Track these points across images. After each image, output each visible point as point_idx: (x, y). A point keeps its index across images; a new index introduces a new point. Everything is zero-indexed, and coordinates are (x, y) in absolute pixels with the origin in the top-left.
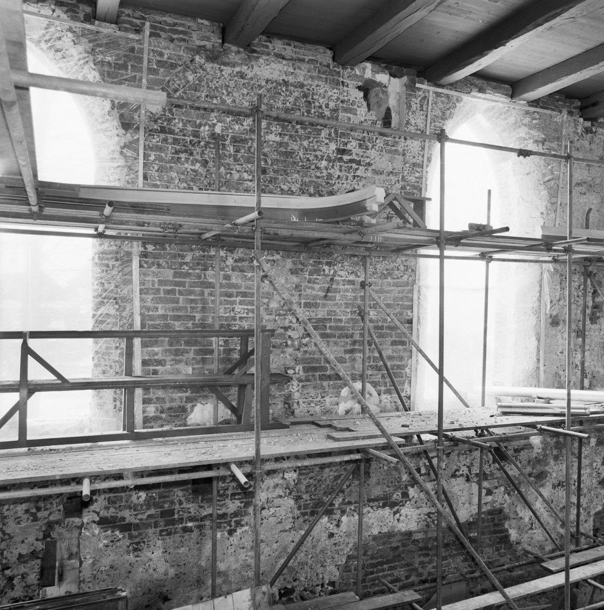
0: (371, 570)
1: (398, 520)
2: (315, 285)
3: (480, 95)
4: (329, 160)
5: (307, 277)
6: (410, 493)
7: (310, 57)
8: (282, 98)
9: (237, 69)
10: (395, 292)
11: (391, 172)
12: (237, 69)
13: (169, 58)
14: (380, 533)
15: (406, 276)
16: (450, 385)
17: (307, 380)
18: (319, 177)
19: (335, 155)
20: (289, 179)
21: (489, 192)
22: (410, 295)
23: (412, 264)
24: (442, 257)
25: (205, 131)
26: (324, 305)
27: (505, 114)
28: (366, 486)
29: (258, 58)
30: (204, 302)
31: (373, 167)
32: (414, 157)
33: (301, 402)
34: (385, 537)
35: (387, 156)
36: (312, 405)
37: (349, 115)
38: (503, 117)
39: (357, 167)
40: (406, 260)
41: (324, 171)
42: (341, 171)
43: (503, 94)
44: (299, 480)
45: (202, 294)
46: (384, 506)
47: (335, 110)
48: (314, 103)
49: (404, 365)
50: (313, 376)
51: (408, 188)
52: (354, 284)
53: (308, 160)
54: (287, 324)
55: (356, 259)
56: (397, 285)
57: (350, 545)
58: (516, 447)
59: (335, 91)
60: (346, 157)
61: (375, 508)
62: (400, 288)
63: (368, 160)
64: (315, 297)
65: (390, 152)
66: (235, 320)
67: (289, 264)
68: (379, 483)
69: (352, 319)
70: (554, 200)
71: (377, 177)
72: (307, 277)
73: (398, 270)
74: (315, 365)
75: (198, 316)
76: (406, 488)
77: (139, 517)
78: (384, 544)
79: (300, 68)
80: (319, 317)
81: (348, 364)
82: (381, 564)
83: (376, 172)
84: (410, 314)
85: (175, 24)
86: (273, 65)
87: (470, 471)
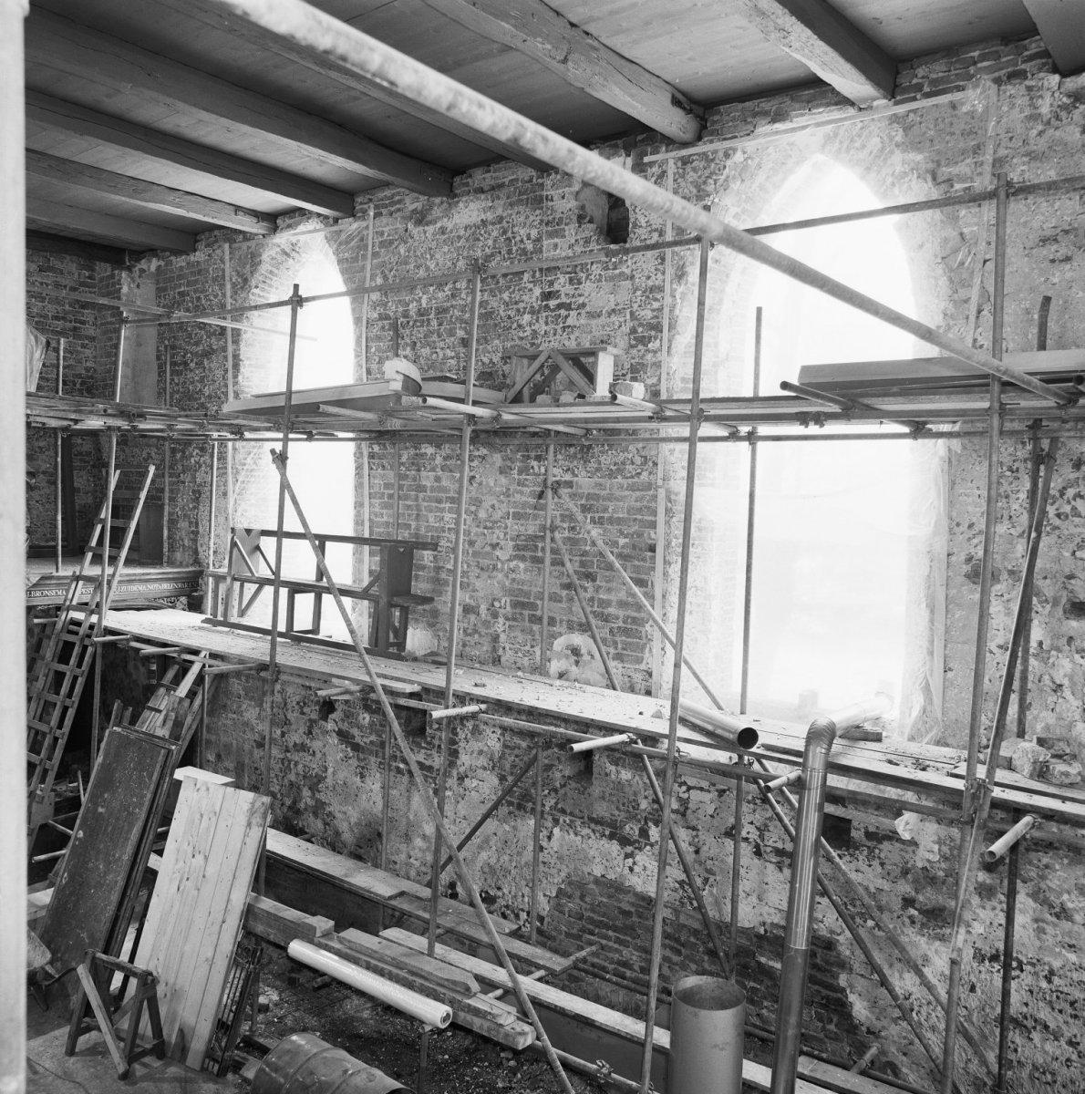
0: (591, 927)
1: (631, 869)
2: (525, 489)
3: (779, 126)
4: (532, 312)
5: (516, 476)
6: (651, 833)
7: (510, 178)
8: (481, 244)
9: (439, 225)
10: (631, 499)
11: (613, 310)
12: (439, 225)
13: (389, 235)
14: (603, 876)
15: (645, 474)
16: (690, 668)
17: (514, 619)
18: (522, 339)
19: (539, 302)
20: (489, 347)
21: (759, 310)
22: (653, 504)
23: (653, 453)
24: (692, 441)
25: (413, 307)
26: (536, 517)
27: (860, 136)
28: (586, 796)
29: (458, 202)
30: (418, 508)
31: (588, 309)
32: (649, 278)
33: (507, 648)
34: (611, 886)
35: (606, 286)
36: (520, 654)
37: (556, 240)
38: (857, 145)
39: (566, 313)
40: (644, 448)
41: (528, 328)
42: (547, 324)
43: (828, 105)
44: (504, 754)
45: (416, 499)
46: (612, 837)
47: (538, 240)
48: (514, 238)
49: (643, 619)
50: (521, 614)
51: (640, 330)
52: (572, 487)
53: (509, 317)
54: (495, 541)
55: (572, 450)
56: (632, 488)
57: (563, 874)
58: (872, 829)
59: (538, 212)
60: (552, 303)
61: (597, 835)
62: (638, 493)
63: (581, 300)
64: (524, 505)
65: (612, 278)
66: (444, 531)
67: (497, 459)
68: (603, 798)
69: (569, 539)
70: (962, 293)
71: (594, 322)
72: (516, 476)
73: (633, 463)
74: (522, 599)
75: (413, 524)
76: (646, 823)
77: (365, 740)
78: (610, 897)
79: (498, 198)
80: (530, 532)
81: (564, 605)
82: (608, 928)
83: (592, 315)
84: (653, 536)
85: (393, 195)
86: (472, 206)
87: (761, 837)
